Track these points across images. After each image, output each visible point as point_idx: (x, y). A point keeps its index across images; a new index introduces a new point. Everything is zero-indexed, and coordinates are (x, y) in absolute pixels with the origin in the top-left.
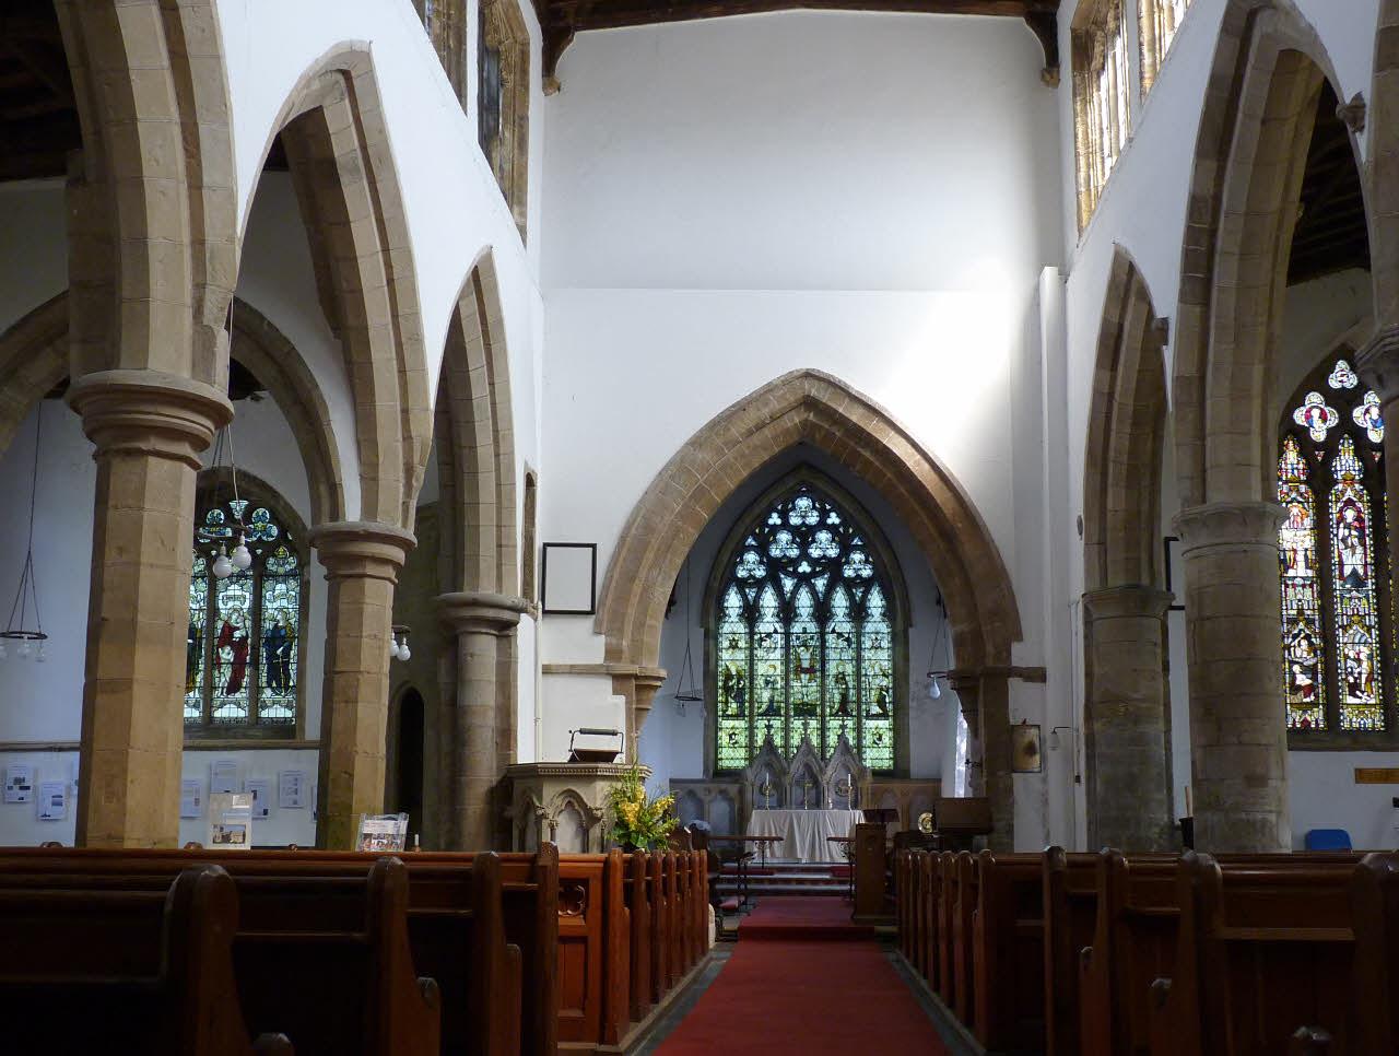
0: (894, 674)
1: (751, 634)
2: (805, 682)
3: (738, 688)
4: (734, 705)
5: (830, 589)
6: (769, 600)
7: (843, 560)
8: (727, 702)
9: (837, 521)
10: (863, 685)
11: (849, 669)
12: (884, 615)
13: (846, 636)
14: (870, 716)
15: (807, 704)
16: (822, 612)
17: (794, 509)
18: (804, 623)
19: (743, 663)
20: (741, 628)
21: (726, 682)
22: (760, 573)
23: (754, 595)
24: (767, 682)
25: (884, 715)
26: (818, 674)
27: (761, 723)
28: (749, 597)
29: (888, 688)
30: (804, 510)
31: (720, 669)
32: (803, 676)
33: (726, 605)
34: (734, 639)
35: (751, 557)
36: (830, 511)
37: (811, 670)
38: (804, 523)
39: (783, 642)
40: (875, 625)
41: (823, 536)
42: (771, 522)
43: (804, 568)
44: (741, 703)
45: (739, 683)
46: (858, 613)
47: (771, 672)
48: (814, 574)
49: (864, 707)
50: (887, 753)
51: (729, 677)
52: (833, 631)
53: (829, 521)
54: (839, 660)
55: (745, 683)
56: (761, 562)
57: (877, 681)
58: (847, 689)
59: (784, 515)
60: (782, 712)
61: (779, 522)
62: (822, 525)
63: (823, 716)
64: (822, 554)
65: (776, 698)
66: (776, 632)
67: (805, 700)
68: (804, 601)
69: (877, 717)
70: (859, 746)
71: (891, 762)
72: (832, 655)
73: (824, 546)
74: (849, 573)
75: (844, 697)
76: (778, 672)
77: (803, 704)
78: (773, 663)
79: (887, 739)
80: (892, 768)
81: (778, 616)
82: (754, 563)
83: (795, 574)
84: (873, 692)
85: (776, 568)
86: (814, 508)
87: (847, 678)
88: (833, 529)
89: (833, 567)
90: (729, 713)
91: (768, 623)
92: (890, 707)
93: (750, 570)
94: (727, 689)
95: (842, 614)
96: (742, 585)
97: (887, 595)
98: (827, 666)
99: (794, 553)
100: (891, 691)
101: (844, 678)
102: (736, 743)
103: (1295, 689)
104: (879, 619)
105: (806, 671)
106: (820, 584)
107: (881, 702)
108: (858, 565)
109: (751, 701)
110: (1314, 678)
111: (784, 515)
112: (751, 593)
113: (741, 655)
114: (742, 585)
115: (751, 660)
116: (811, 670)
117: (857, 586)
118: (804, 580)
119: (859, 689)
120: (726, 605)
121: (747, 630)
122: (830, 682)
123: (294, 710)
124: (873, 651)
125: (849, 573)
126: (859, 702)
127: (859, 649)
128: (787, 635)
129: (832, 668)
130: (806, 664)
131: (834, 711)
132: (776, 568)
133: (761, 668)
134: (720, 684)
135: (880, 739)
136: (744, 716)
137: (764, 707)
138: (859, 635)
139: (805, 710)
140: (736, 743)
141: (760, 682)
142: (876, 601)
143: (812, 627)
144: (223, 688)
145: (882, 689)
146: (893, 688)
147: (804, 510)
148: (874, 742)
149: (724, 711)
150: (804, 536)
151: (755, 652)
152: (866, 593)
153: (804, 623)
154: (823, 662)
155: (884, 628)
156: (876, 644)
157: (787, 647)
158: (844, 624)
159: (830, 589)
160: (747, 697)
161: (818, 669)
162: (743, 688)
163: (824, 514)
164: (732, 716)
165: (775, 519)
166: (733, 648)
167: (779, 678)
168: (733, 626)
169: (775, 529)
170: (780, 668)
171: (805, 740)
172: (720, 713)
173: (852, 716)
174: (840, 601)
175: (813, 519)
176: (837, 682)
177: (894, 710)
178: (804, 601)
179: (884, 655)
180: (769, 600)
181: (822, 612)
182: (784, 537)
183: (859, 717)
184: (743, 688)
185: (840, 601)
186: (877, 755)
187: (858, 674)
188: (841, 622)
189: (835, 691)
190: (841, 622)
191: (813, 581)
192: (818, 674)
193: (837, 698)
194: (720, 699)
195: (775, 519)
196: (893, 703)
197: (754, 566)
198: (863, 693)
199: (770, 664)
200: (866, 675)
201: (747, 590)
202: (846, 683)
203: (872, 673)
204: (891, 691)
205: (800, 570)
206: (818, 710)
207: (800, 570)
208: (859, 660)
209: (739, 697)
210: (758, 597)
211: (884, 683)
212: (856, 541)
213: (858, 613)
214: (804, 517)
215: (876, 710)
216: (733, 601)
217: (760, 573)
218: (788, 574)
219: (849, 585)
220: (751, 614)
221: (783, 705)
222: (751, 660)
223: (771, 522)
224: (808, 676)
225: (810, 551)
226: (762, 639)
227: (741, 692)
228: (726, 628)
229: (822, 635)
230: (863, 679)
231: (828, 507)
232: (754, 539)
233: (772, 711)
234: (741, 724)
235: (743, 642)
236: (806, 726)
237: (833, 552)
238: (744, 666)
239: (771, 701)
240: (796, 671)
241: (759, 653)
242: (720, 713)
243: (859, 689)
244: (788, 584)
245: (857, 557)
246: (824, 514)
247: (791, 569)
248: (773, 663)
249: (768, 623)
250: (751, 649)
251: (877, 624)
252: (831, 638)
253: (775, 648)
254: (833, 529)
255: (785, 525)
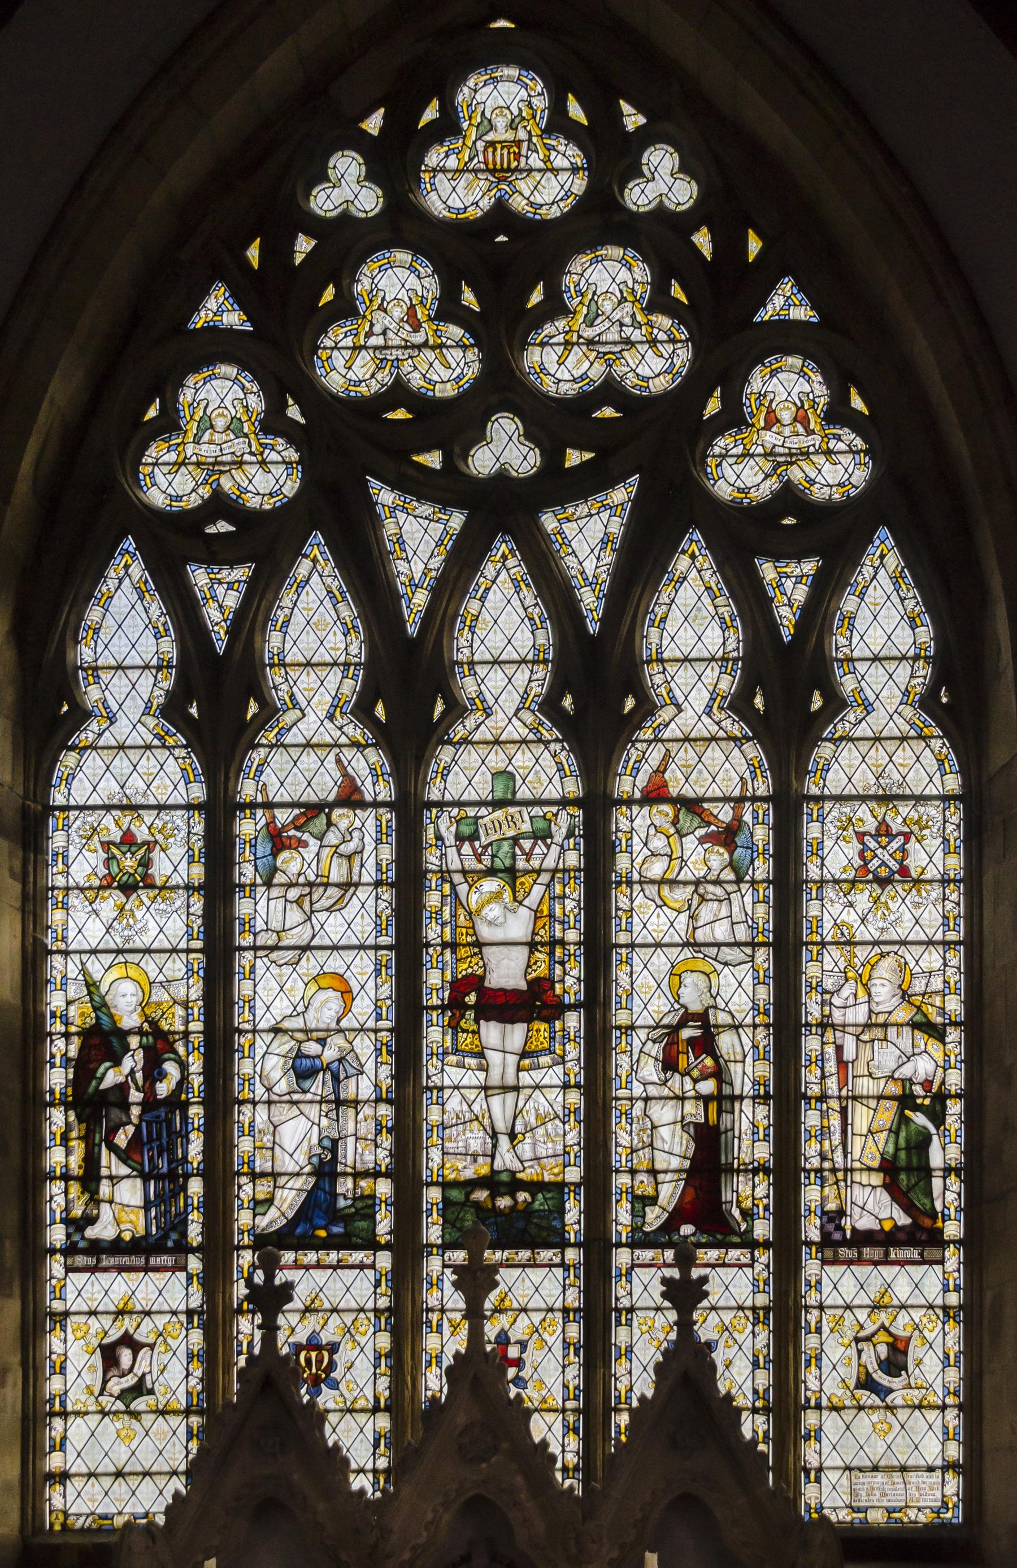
0: (974, 1022)
1: (219, 812)
2: (501, 1065)
3: (150, 1103)
4: (130, 1192)
5: (640, 566)
6: (315, 628)
7: (713, 406)
8: (90, 1178)
9: (683, 194)
10: (810, 1079)
11: (739, 991)
12: (172, 710)
13: (725, 814)
14: (844, 1243)
15: (515, 1185)
16: (597, 691)
17: (448, 127)
18: (501, 751)
19: (176, 966)
20: (169, 776)
21: (84, 1069)
22: (269, 480)
23: (232, 600)
24: (303, 1070)
25: (921, 1237)
26: (573, 1021)
27: (642, 1284)
28: (212, 614)
29: (941, 1098)
30: (504, 138)
31: (56, 1001)
32: (491, 1032)
33: (86, 654)
34: (128, 840)
35: (221, 395)
36: (645, 138)
37: (532, 1003)
38: (500, 207)
39: (387, 853)
40: (878, 755)
41: (607, 278)
42: (324, 202)
43: (504, 449)
44: (165, 1185)
45: (153, 1071)
46: (787, 694)
47: (326, 1009)
48: (557, 486)
49: (811, 1194)
50: (931, 1439)
51: (102, 1041)
52: (655, 794)
53: (639, 197)
54: (684, 942)
55: (186, 1070)
56: (273, 423)
57: (886, 1058)
58: (724, 1100)
59: (395, 165)
60: (384, 1225)
61: (369, 201)
62: (599, 219)
63: (598, 1245)
64: (597, 371)
65: (350, 1154)
66: (350, 797)
67: (505, 1159)
68: (503, 629)
69: (879, 1244)
70: (786, 1405)
71: (953, 1484)
72: (647, 918)
73: (610, 330)
74: (737, 475)
75: (709, 1145)
76: (363, 1007)
77: (492, 1182)
78: (335, 963)
79: (935, 1363)
80: (953, 1515)
81: (363, 711)
82: (234, 427)
83: (448, 488)
84: (861, 1117)
85: (352, 454)
86: (558, 124)
87: (726, 1042)
88: (657, 238)
89: (650, 449)
90: (103, 1230)
91: (313, 741)
92: (948, 1195)
93: (214, 467)
94: (93, 1107)
95: (699, 699)
96: (174, 545)
97: (947, 587)
98: (621, 975)
99: (448, 369)
100: (955, 1108)
101: (706, 1044)
102: (139, 1389)
103: (565, 1469)
104: (517, 730)
105: (503, 1006)
106: (588, 537)
107: (904, 1172)
108: (791, 435)
109: (220, 1171)
110: (943, 1215)
111: (395, 165)
112: (788, 584)
113: (169, 923)
114: (174, 545)
115: (219, 952)
116: (532, 1003)
117: (218, 553)
118: (501, 515)
119: (786, 1097)
120: (86, 654)
121: (198, 792)
122: (636, 1065)
123: (953, 1258)
124: (862, 899)
125: (737, 475)
126: (786, 1171)
127: (788, 889)
128: (409, 813)
129: (645, 994)
130: (507, 971)
131: (654, 1217)
132: (352, 454)
133: (271, 994)
134: (57, 1079)
135: (896, 1361)
136: (183, 1248)
137: (289, 1198)
138: (788, 808)
139: (504, 1218)
140: (139, 1389)
141: (264, 1064)
142: (883, 623)
143: (547, 772)
144: (65, 1139)
145: (906, 1101)
146: (973, 1095)
147: (504, 138)
148: (867, 1383)
149: (77, 1225)
150: (500, 274)
151: (243, 907)
152: (827, 589)
153: (501, 751)
154: (599, 952)
155: (927, 768)
156: (885, 857)
157: (408, 881)
158: (714, 754)
159: (640, 566)
160: (195, 1147)
161: (572, 998)
162: (177, 1102)
163: (611, 158)
164: (116, 1246)
165: (347, 188)
166: (128, 889)
167: (364, 1046)
168: (124, 767)
169: (348, 244)
170: (372, 992)
171: (688, 1365)
172: (57, 1235)
173: (750, 1244)
174: (691, 625)
175: (551, 186)
176: (669, 1064)
177: (973, 1208)
178: (503, 629)
179: (926, 915)
180: (315, 628)
181: (597, 691)
182: (397, 282)
183: (787, 1248)
184: (177, 1102)
185: (691, 625)
186: (876, 1450)
187: (786, 1023)
188: (696, 734)
189: (664, 1113)
190: (696, 734)
191: (549, 522)
192: (573, 1021)
193: (674, 1149)
194: (55, 1157)
195: (347, 188)
196: (972, 1170)
197: (240, 445)
198: (811, 1119)
199: (315, 977)
200: (825, 1025)
201: (768, 571)
202: (719, 1074)
203: (859, 1014)
204: (955, 1108)
205: (482, 462)
206: (573, 1212)
207: (482, 462)
208: (787, 944)
209: (155, 1154)
210: (819, 611)
211: (923, 1067)
212: (786, 303)
213: (787, 694)
214: (501, 174)
215: (873, 1207)
216: (124, 633)
217: (269, 480)
218: (417, 486)
219: (745, 538)
220: (218, 702)
221: (384, 1188)
222: (219, 952)
223: (324, 202)
224: (517, 1034)
225: (533, 356)
226: (279, 841)
227: (164, 1116)
228: (85, 778)
229: (596, 807)
230: (811, 1044)
231: (633, 119)
232: (240, 298)
233: (327, 1221)
234: (169, 1291)
235: (177, 851)
236: (686, 1295)
237: (655, 365)
238: (181, 983)
239: (326, 1170)
240: (455, 1005)
241: (261, 911)
242: (57, 1235)
243: (786, 1097)
244: (417, 537)
245: (787, 385)
246: (611, 158)
247: (433, 460)
248: (335, 963)
249: (313, 741)
250: (218, 889)
251: (887, 753)
252: (642, 835)
253: (348, 886)
254: (657, 238)
255: (402, 223)
